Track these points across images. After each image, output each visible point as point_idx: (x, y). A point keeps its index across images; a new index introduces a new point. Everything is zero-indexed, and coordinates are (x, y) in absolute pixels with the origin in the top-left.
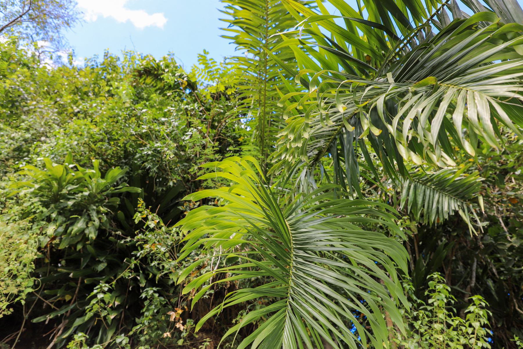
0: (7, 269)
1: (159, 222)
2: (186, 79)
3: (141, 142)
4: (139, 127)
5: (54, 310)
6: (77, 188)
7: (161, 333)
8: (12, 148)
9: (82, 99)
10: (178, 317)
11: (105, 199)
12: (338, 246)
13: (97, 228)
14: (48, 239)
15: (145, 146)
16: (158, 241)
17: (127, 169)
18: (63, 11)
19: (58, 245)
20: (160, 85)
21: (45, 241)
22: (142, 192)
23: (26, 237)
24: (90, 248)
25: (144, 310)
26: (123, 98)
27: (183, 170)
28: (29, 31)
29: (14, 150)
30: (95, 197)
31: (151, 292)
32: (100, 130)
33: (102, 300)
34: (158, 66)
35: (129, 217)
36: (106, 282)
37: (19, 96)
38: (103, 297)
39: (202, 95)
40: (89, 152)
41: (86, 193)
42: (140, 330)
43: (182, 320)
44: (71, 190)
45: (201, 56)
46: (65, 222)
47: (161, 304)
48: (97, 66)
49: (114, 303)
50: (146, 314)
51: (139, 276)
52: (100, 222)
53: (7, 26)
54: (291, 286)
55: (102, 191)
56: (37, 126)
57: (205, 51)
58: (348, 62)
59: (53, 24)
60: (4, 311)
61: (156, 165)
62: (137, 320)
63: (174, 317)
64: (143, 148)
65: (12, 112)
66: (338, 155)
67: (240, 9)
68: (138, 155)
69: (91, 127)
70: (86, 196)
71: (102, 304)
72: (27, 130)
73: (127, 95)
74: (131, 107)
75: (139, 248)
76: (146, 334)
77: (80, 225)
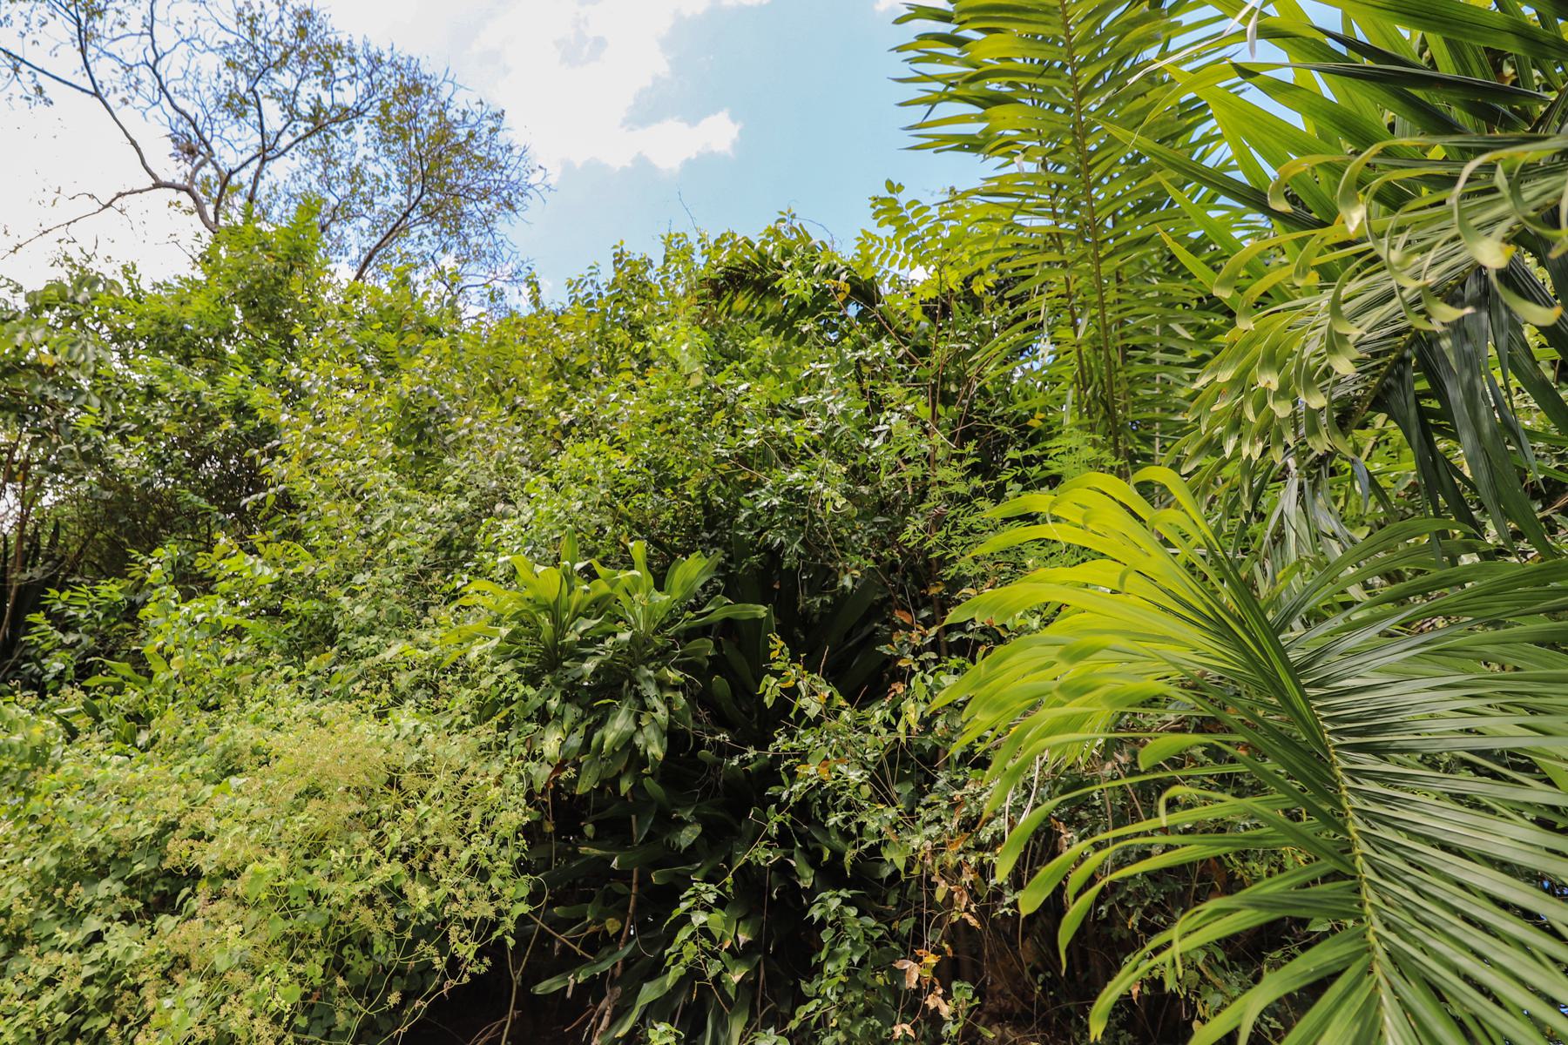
0: (465, 856)
1: (831, 695)
2: (843, 276)
3: (747, 475)
4: (734, 435)
5: (580, 962)
6: (600, 625)
7: (878, 1024)
9: (574, 389)
10: (928, 975)
11: (674, 647)
12: (1505, 731)
14: (549, 770)
15: (759, 484)
16: (836, 754)
17: (718, 555)
18: (497, 177)
19: (573, 782)
20: (772, 308)
21: (542, 774)
22: (769, 616)
23: (496, 768)
24: (651, 785)
25: (823, 956)
26: (682, 363)
27: (874, 538)
28: (426, 247)
30: (647, 642)
31: (835, 903)
32: (636, 460)
33: (705, 931)
34: (763, 257)
35: (746, 691)
36: (707, 880)
37: (432, 409)
38: (706, 921)
39: (897, 312)
40: (615, 527)
41: (625, 636)
42: (817, 1015)
43: (942, 986)
44: (586, 631)
45: (883, 200)
46: (583, 720)
47: (868, 938)
48: (600, 295)
49: (736, 937)
50: (830, 967)
51: (791, 857)
52: (671, 712)
53: (379, 245)
54: (1368, 880)
55: (662, 627)
56: (481, 479)
57: (889, 184)
58: (1418, 93)
59: (478, 214)
60: (470, 964)
61: (798, 533)
62: (804, 986)
63: (916, 977)
65: (419, 453)
66: (1423, 413)
67: (979, 36)
68: (744, 514)
69: (613, 457)
71: (706, 943)
72: (459, 491)
73: (692, 354)
74: (706, 383)
75: (785, 778)
76: (837, 1027)
77: (619, 725)
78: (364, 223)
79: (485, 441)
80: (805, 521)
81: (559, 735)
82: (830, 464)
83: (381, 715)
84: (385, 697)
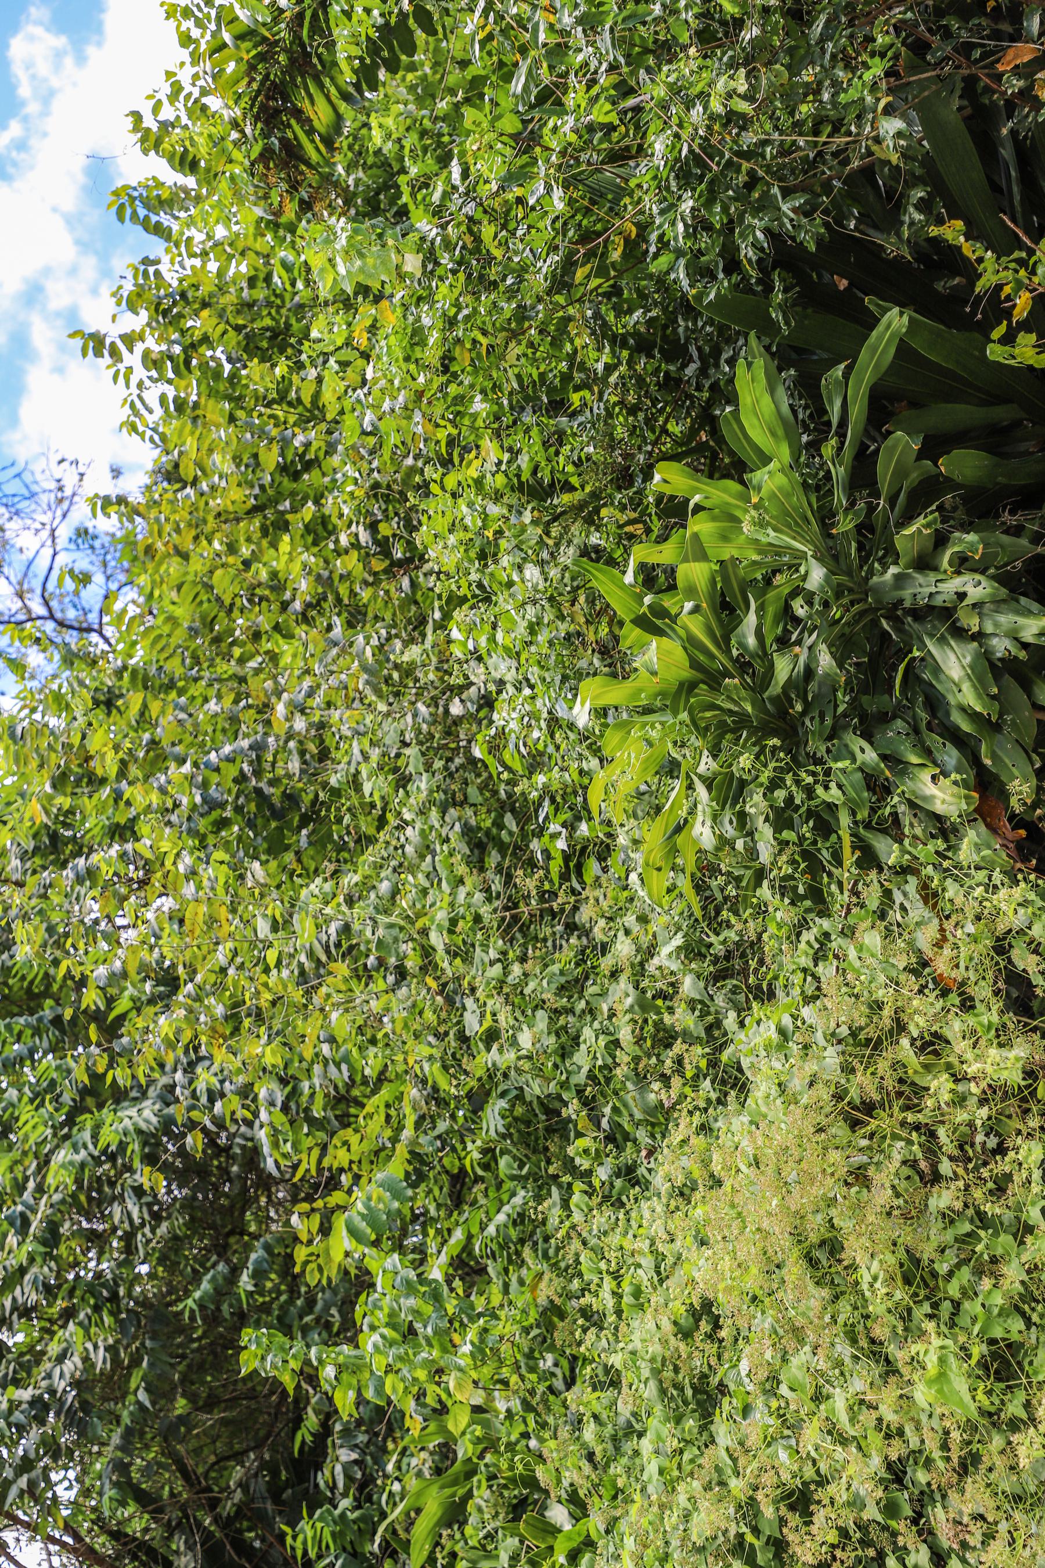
13: (1004, 592)
15: (643, 228)
55: (826, 517)
64: (654, 237)
69: (473, 473)
70: (827, 579)
77: (954, 665)
80: (751, 173)
81: (926, 775)
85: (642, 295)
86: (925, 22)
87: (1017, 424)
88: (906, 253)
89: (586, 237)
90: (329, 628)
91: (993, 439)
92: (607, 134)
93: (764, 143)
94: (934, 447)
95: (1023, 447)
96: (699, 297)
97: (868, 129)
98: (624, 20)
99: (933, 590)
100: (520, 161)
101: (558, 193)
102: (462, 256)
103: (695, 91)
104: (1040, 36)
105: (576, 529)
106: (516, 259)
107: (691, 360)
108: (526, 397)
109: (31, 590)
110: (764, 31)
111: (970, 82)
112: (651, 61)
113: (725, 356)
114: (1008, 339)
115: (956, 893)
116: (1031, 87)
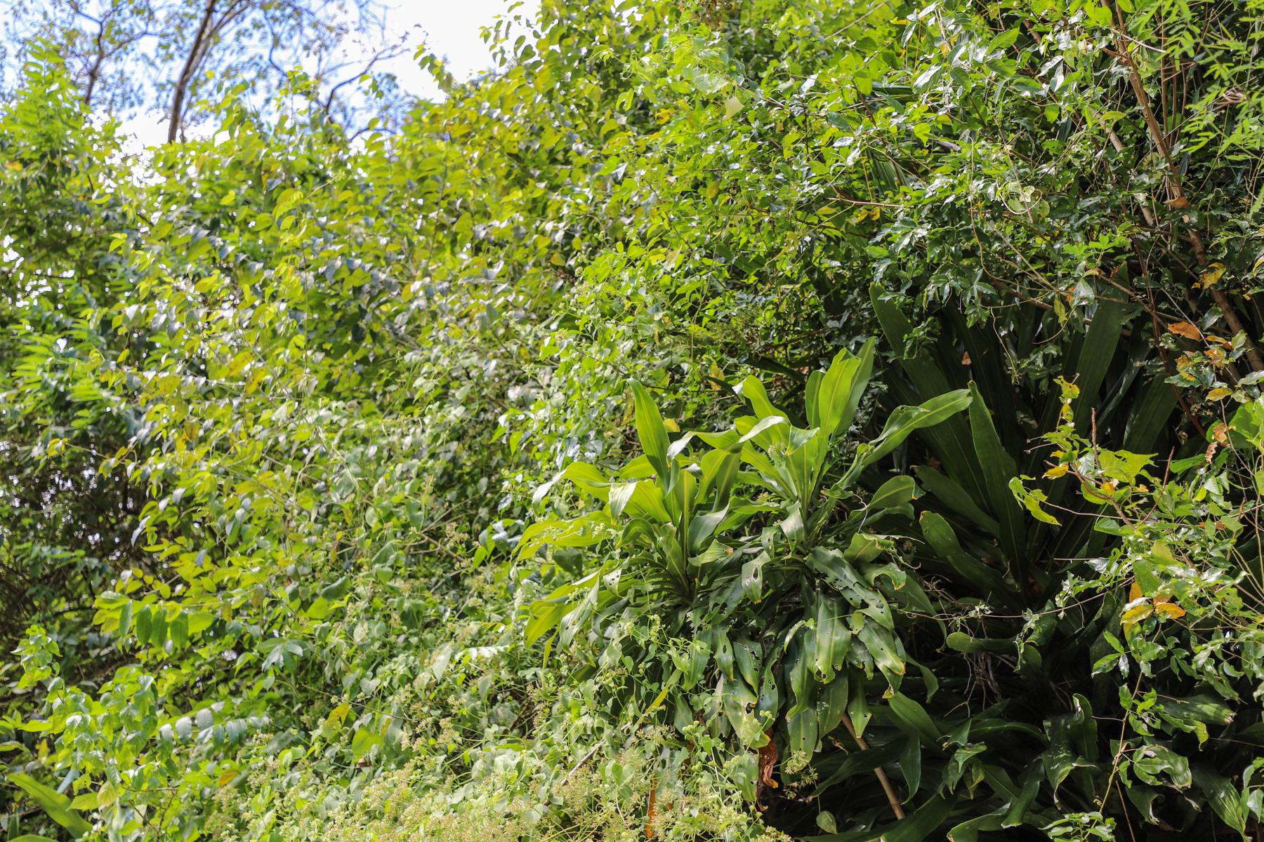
8: (428, 487)
13: (890, 625)
15: (885, 220)
29: (440, 488)
53: (187, 71)
55: (826, 482)
64: (886, 231)
69: (654, 260)
72: (443, 397)
78: (148, 45)
79: (450, 313)
82: (982, 147)
83: (461, 770)
84: (450, 737)
85: (848, 256)
86: (1151, 259)
87: (990, 537)
88: (1015, 376)
89: (848, 192)
90: (490, 265)
91: (968, 533)
92: (916, 147)
93: (999, 239)
94: (929, 502)
95: (980, 553)
96: (878, 292)
97: (1063, 288)
98: (1017, 84)
99: (851, 586)
100: (850, 113)
101: (855, 154)
102: (766, 133)
103: (985, 171)
104: (1208, 330)
105: (681, 349)
106: (794, 168)
107: (839, 319)
108: (724, 249)
109: (327, 82)
110: (1057, 176)
111: (1146, 317)
112: (979, 129)
113: (858, 338)
114: (1029, 486)
115: (706, 784)
116: (1178, 354)
